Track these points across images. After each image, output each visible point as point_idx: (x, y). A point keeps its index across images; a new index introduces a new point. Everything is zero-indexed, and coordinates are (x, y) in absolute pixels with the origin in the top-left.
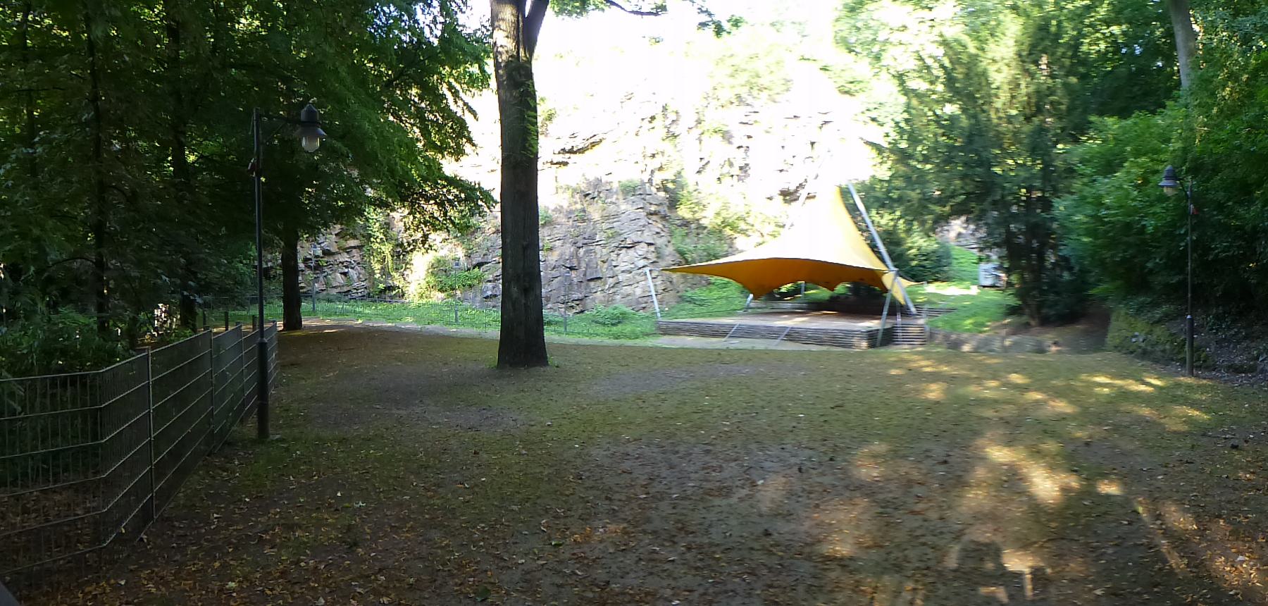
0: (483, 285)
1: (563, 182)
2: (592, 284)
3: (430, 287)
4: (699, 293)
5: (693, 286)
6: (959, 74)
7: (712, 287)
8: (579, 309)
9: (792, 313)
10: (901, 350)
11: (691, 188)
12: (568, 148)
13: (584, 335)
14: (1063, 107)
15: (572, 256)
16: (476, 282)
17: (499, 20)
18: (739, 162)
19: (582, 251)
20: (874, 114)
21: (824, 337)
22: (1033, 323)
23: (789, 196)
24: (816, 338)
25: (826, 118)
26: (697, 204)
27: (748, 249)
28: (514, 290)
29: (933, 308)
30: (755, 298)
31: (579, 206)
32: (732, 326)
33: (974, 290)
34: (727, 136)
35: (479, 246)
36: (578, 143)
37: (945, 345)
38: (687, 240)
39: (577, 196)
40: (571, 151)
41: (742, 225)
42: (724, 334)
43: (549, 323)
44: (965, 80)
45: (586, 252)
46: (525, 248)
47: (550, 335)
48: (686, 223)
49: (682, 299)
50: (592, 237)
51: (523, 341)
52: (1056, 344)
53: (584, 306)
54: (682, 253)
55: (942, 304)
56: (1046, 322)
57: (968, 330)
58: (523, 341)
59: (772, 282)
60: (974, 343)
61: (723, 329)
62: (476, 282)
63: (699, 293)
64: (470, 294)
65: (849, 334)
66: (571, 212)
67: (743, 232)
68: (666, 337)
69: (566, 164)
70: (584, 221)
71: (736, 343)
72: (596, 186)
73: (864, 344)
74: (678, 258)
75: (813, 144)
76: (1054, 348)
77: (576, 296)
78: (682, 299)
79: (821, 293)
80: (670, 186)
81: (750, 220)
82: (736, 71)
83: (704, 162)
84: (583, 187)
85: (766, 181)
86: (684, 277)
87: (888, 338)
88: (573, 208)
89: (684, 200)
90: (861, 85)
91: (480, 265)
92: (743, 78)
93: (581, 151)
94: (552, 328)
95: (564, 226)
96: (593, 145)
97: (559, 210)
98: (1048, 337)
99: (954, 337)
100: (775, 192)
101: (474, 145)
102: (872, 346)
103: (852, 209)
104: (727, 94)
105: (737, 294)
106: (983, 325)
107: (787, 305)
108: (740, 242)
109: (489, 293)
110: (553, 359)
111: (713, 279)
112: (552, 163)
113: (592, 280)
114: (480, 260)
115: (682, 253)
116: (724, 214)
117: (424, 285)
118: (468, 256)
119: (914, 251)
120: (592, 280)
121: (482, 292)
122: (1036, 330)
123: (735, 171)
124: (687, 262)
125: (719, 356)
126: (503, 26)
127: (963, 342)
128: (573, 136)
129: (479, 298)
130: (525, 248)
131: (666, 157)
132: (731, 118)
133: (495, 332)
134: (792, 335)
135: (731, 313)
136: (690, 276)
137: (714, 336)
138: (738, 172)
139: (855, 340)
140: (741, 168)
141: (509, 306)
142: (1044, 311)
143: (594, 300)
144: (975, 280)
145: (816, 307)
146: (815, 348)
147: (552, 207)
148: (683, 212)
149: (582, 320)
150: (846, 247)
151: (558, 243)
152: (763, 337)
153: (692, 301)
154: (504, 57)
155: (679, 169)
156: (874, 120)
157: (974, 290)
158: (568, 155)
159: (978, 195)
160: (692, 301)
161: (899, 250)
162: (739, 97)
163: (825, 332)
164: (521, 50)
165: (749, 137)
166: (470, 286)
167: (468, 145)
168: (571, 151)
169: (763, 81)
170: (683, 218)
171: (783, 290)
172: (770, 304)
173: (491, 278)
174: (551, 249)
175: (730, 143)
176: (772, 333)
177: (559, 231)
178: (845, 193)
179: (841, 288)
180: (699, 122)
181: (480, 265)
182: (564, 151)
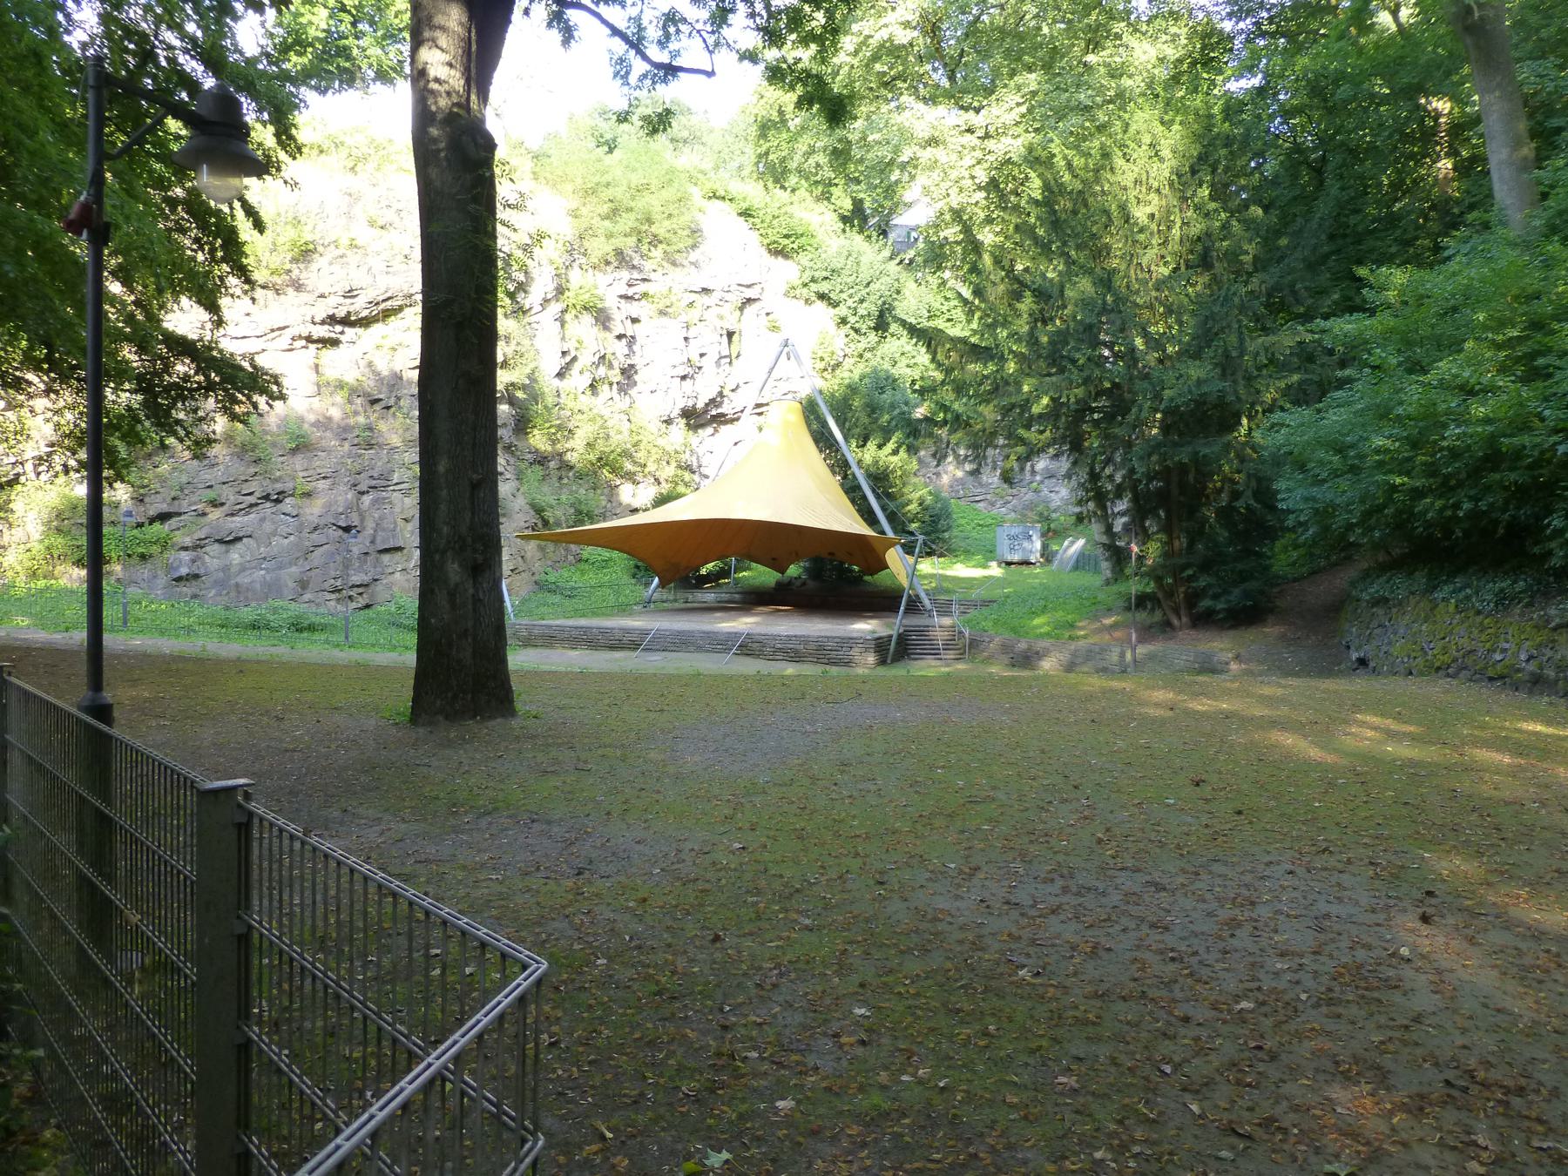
0: (171, 555)
1: (331, 374)
2: (386, 558)
3: (51, 556)
4: (567, 576)
5: (555, 565)
6: (1064, 204)
7: (583, 566)
8: (362, 601)
9: (722, 608)
10: (926, 668)
11: (550, 400)
12: (341, 313)
13: (382, 646)
14: (1247, 258)
15: (349, 507)
16: (155, 549)
17: (433, 27)
18: (620, 361)
19: (367, 499)
20: (824, 287)
21: (821, 648)
22: (1176, 622)
23: (695, 418)
24: (793, 652)
25: (749, 293)
26: (560, 428)
27: (638, 502)
28: (454, 570)
29: (946, 597)
30: (662, 585)
31: (361, 419)
32: (645, 632)
33: (995, 570)
34: (602, 319)
35: (163, 480)
36: (359, 306)
37: (1006, 659)
38: (545, 489)
39: (359, 401)
40: (346, 321)
41: (628, 466)
42: (634, 646)
43: (408, 628)
44: (1068, 219)
45: (375, 502)
46: (475, 486)
47: (518, 659)
48: (541, 460)
49: (540, 586)
50: (385, 477)
51: (461, 665)
52: (1237, 657)
53: (372, 596)
54: (539, 511)
55: (974, 594)
56: (1204, 620)
57: (1048, 634)
58: (461, 665)
59: (689, 559)
60: (1065, 657)
61: (628, 637)
62: (155, 549)
63: (567, 576)
64: (144, 572)
65: (849, 642)
66: (347, 429)
67: (630, 477)
68: (748, 661)
69: (334, 343)
70: (370, 446)
71: (654, 662)
72: (392, 387)
73: (871, 659)
74: (532, 518)
75: (730, 335)
76: (1234, 666)
77: (356, 579)
78: (540, 586)
79: (759, 575)
80: (520, 394)
81: (640, 456)
82: (613, 215)
83: (568, 359)
84: (369, 384)
85: (660, 395)
86: (541, 549)
87: (896, 651)
88: (352, 421)
89: (539, 421)
90: (803, 240)
91: (163, 517)
92: (627, 222)
93: (365, 322)
94: (316, 636)
95: (336, 452)
96: (387, 314)
97: (324, 423)
98: (1220, 646)
99: (1022, 646)
100: (676, 412)
101: (248, 281)
102: (882, 662)
103: (823, 439)
104: (599, 247)
105: (626, 579)
106: (1072, 626)
107: (708, 596)
108: (628, 494)
109: (184, 571)
110: (524, 700)
111: (588, 551)
112: (309, 339)
113: (381, 552)
114: (164, 508)
115: (539, 511)
116: (601, 446)
117: (37, 548)
118: (140, 500)
119: (913, 507)
120: (381, 552)
121: (170, 568)
122: (1186, 635)
123: (615, 375)
124: (546, 523)
125: (632, 683)
126: (443, 41)
127: (1039, 655)
128: (350, 294)
129: (162, 580)
130: (475, 486)
131: (513, 346)
132: (608, 287)
133: (411, 658)
134: (748, 647)
135: (623, 610)
136: (550, 547)
137: (612, 648)
138: (619, 378)
139: (855, 652)
140: (623, 371)
141: (442, 598)
142: (1206, 603)
143: (389, 587)
144: (990, 554)
145: (755, 599)
146: (790, 670)
147: (312, 418)
148: (538, 440)
149: (370, 620)
150: (818, 505)
151: (322, 485)
152: (700, 649)
153: (553, 589)
154: (443, 102)
155: (532, 366)
156: (822, 296)
157: (995, 570)
158: (338, 328)
159: (1089, 421)
160: (553, 589)
161: (892, 506)
162: (619, 253)
163: (804, 640)
164: (473, 97)
165: (635, 321)
166: (143, 557)
167: (232, 281)
168: (346, 321)
169: (660, 229)
170: (537, 451)
171: (703, 571)
172: (681, 595)
173: (188, 541)
174: (308, 495)
175: (606, 328)
176: (721, 644)
177: (323, 463)
178: (810, 410)
179: (793, 570)
180: (560, 291)
181: (163, 517)
182: (332, 320)
